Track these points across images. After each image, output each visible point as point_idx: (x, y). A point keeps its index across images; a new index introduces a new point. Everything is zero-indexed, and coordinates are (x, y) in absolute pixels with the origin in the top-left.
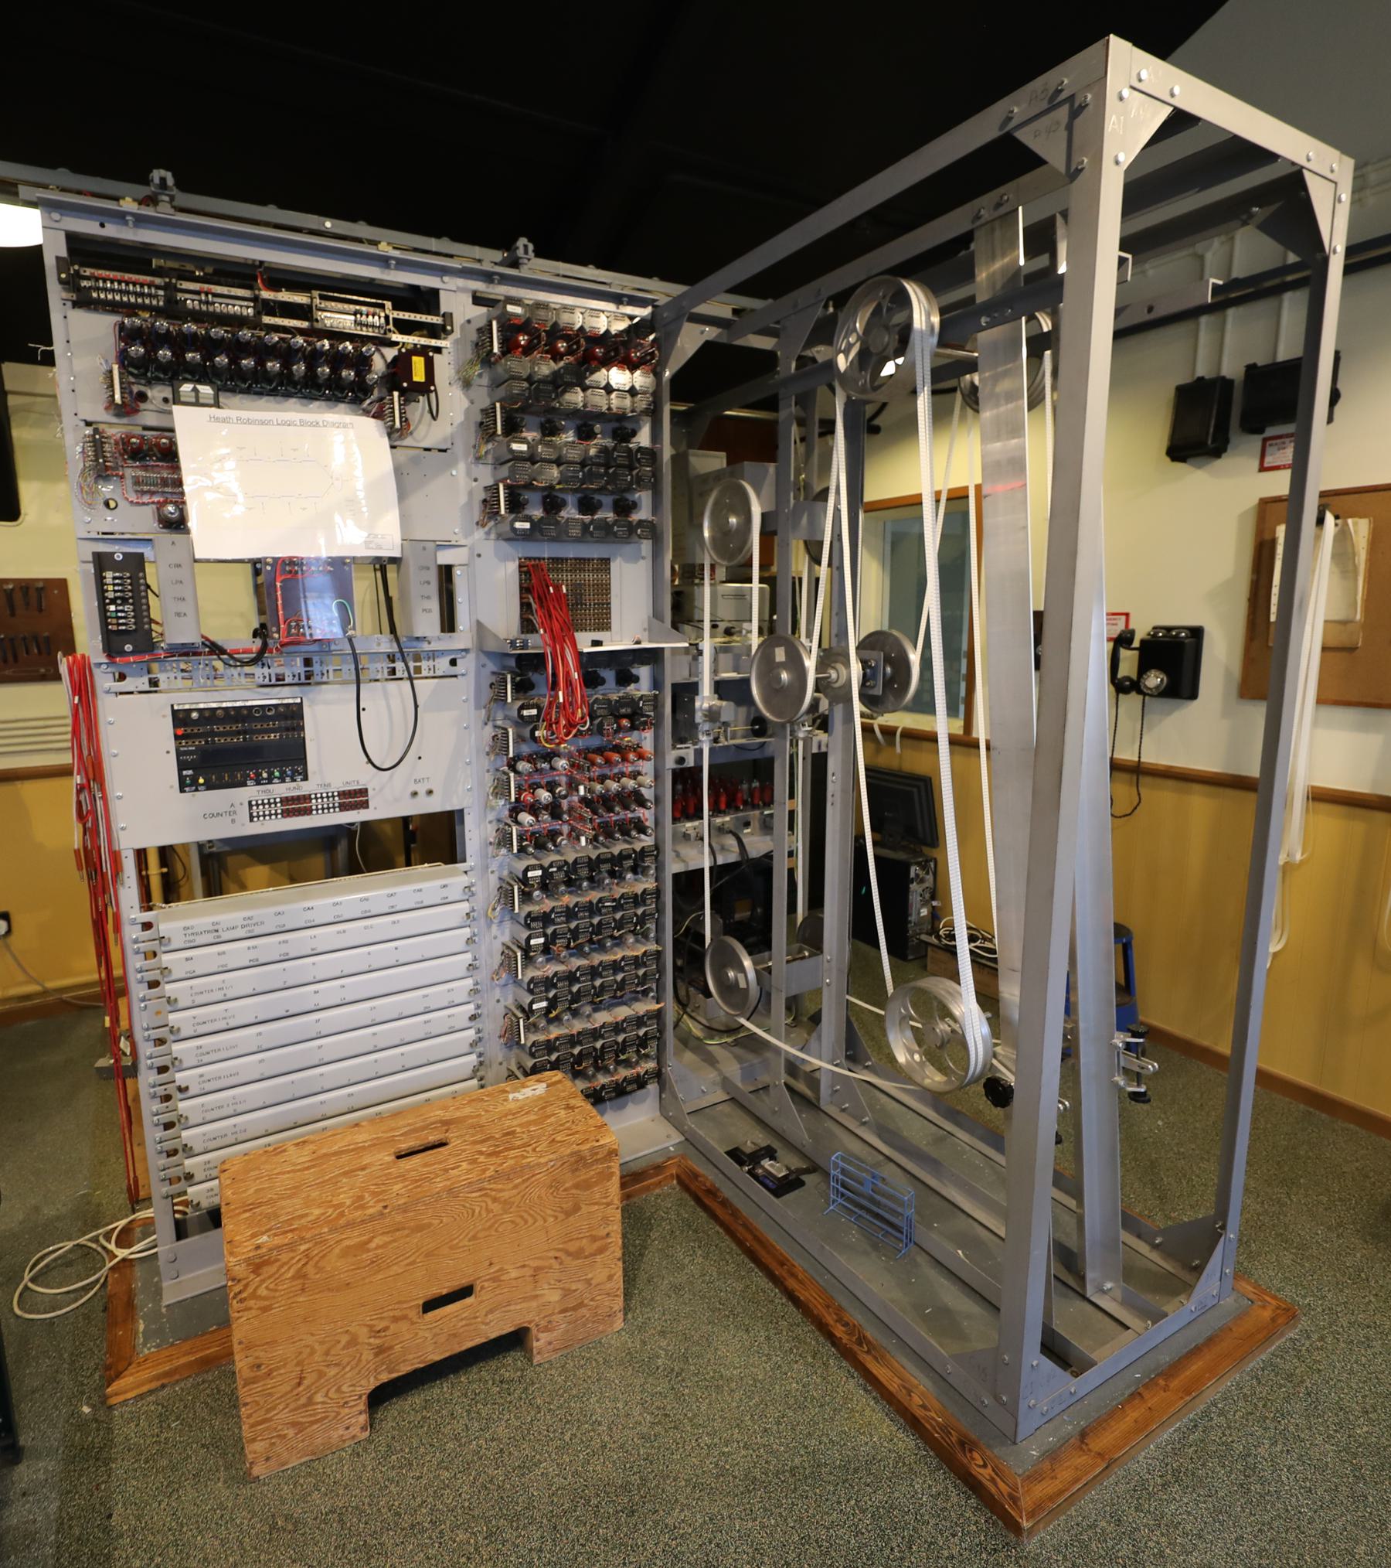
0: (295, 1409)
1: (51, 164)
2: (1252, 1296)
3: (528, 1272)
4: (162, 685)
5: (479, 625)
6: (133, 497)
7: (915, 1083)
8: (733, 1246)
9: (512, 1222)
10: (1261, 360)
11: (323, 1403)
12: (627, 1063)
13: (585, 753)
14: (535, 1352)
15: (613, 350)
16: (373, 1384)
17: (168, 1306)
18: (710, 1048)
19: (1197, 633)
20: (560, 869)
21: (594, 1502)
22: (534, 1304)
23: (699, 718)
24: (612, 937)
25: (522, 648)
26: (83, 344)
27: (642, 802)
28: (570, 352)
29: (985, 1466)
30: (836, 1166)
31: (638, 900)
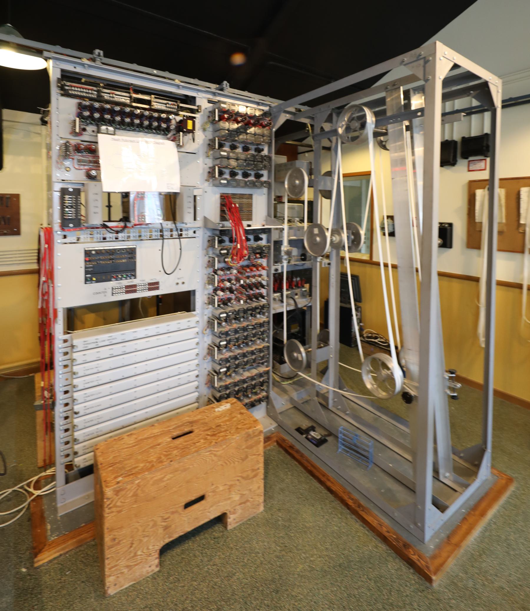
0: (128, 559)
1: (54, 44)
2: (498, 475)
3: (227, 487)
4: (81, 240)
5: (205, 218)
6: (77, 167)
7: (375, 396)
8: (303, 470)
9: (222, 465)
10: (467, 136)
11: (141, 555)
12: (256, 394)
13: (242, 267)
14: (228, 523)
15: (256, 121)
16: (162, 544)
17: (61, 516)
18: (284, 386)
19: (451, 225)
20: (233, 313)
21: (261, 589)
22: (229, 502)
23: (283, 254)
24: (251, 341)
25: (222, 227)
26: (63, 108)
27: (263, 286)
28: (242, 121)
29: (414, 555)
30: (341, 433)
31: (261, 325)
